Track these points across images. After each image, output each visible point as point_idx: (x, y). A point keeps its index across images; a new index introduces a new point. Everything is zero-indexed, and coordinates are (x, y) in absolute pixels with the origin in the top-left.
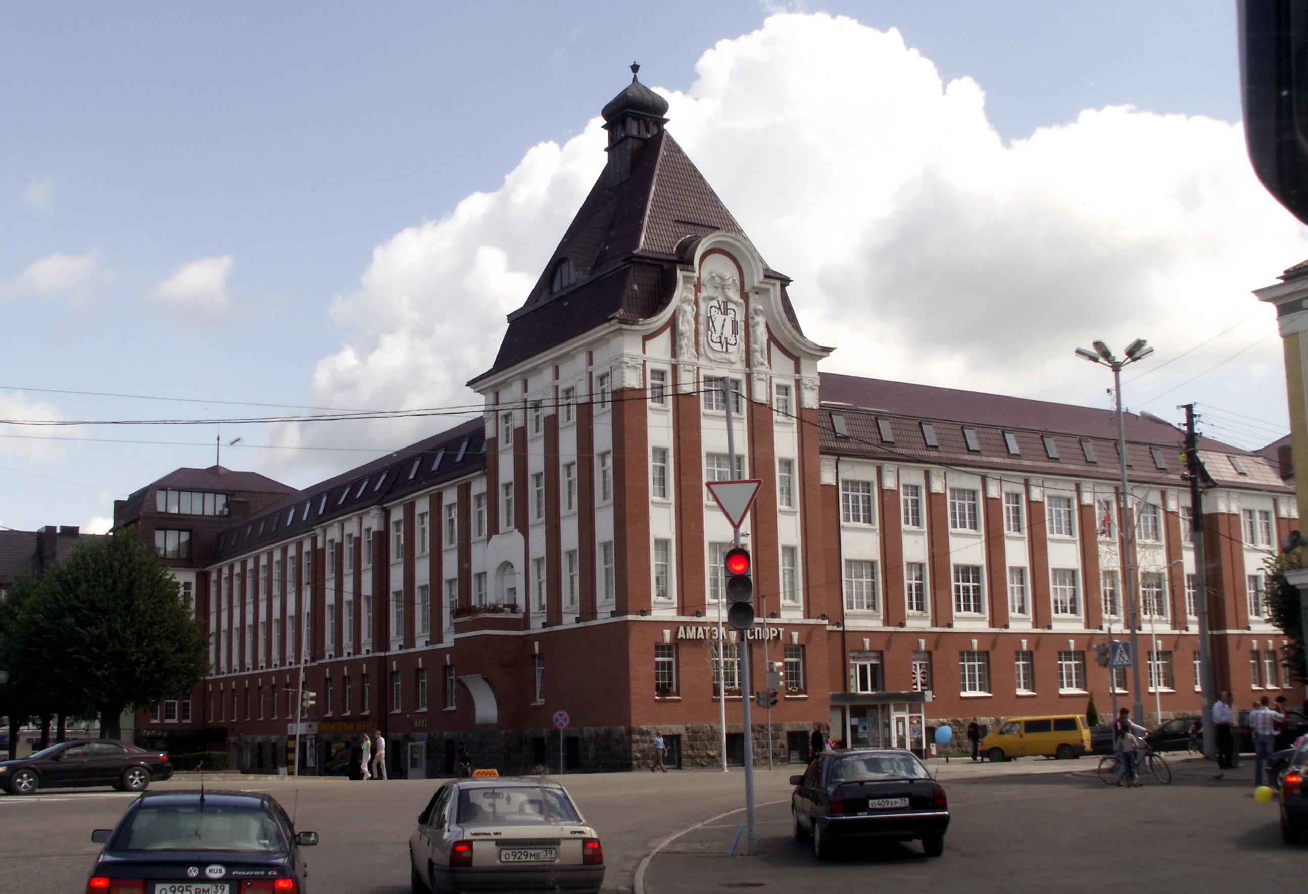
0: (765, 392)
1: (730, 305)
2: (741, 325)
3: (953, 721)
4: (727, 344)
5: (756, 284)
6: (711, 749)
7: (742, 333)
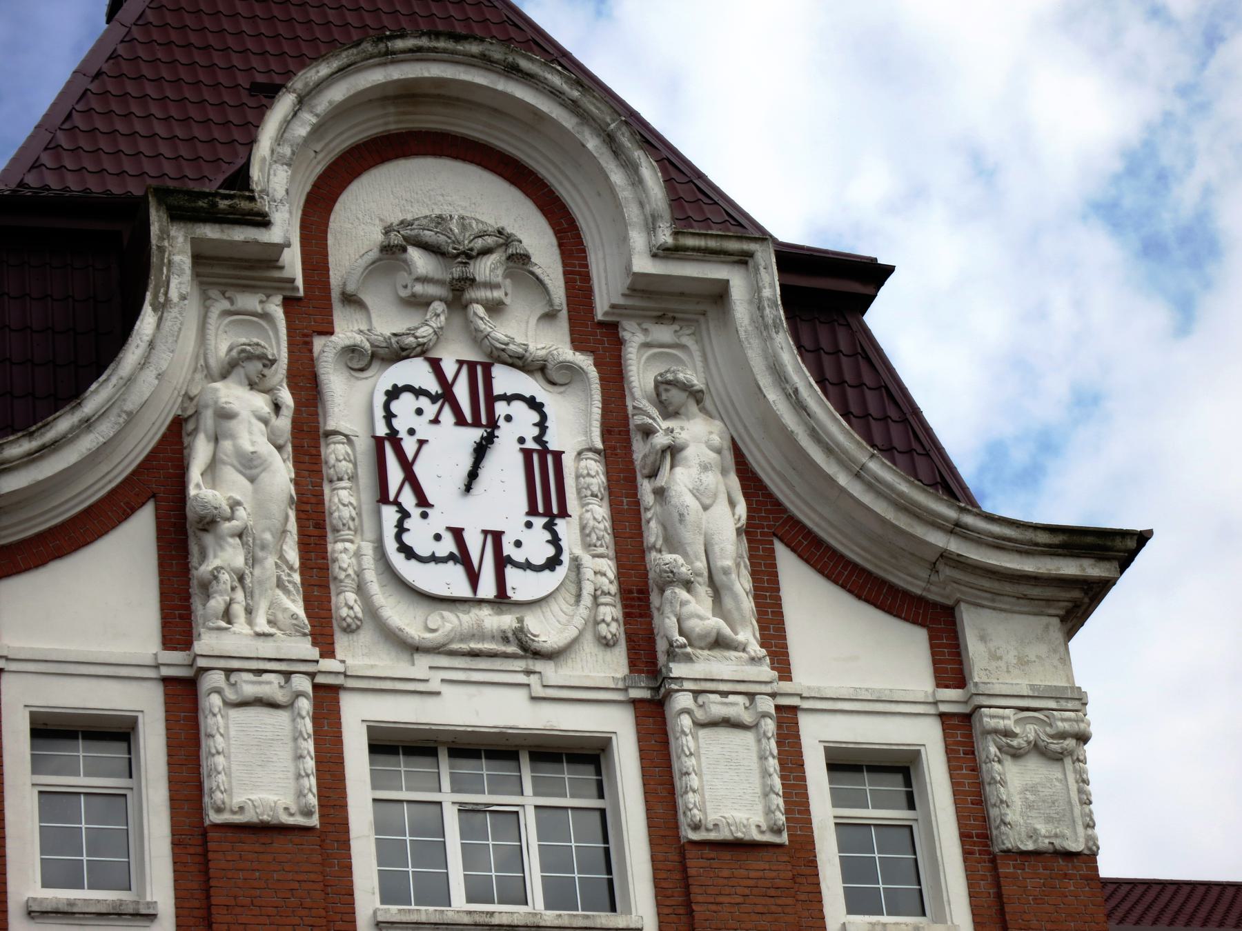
0: (754, 784)
1: (506, 380)
2: (585, 474)
4: (502, 562)
5: (643, 264)
7: (589, 513)
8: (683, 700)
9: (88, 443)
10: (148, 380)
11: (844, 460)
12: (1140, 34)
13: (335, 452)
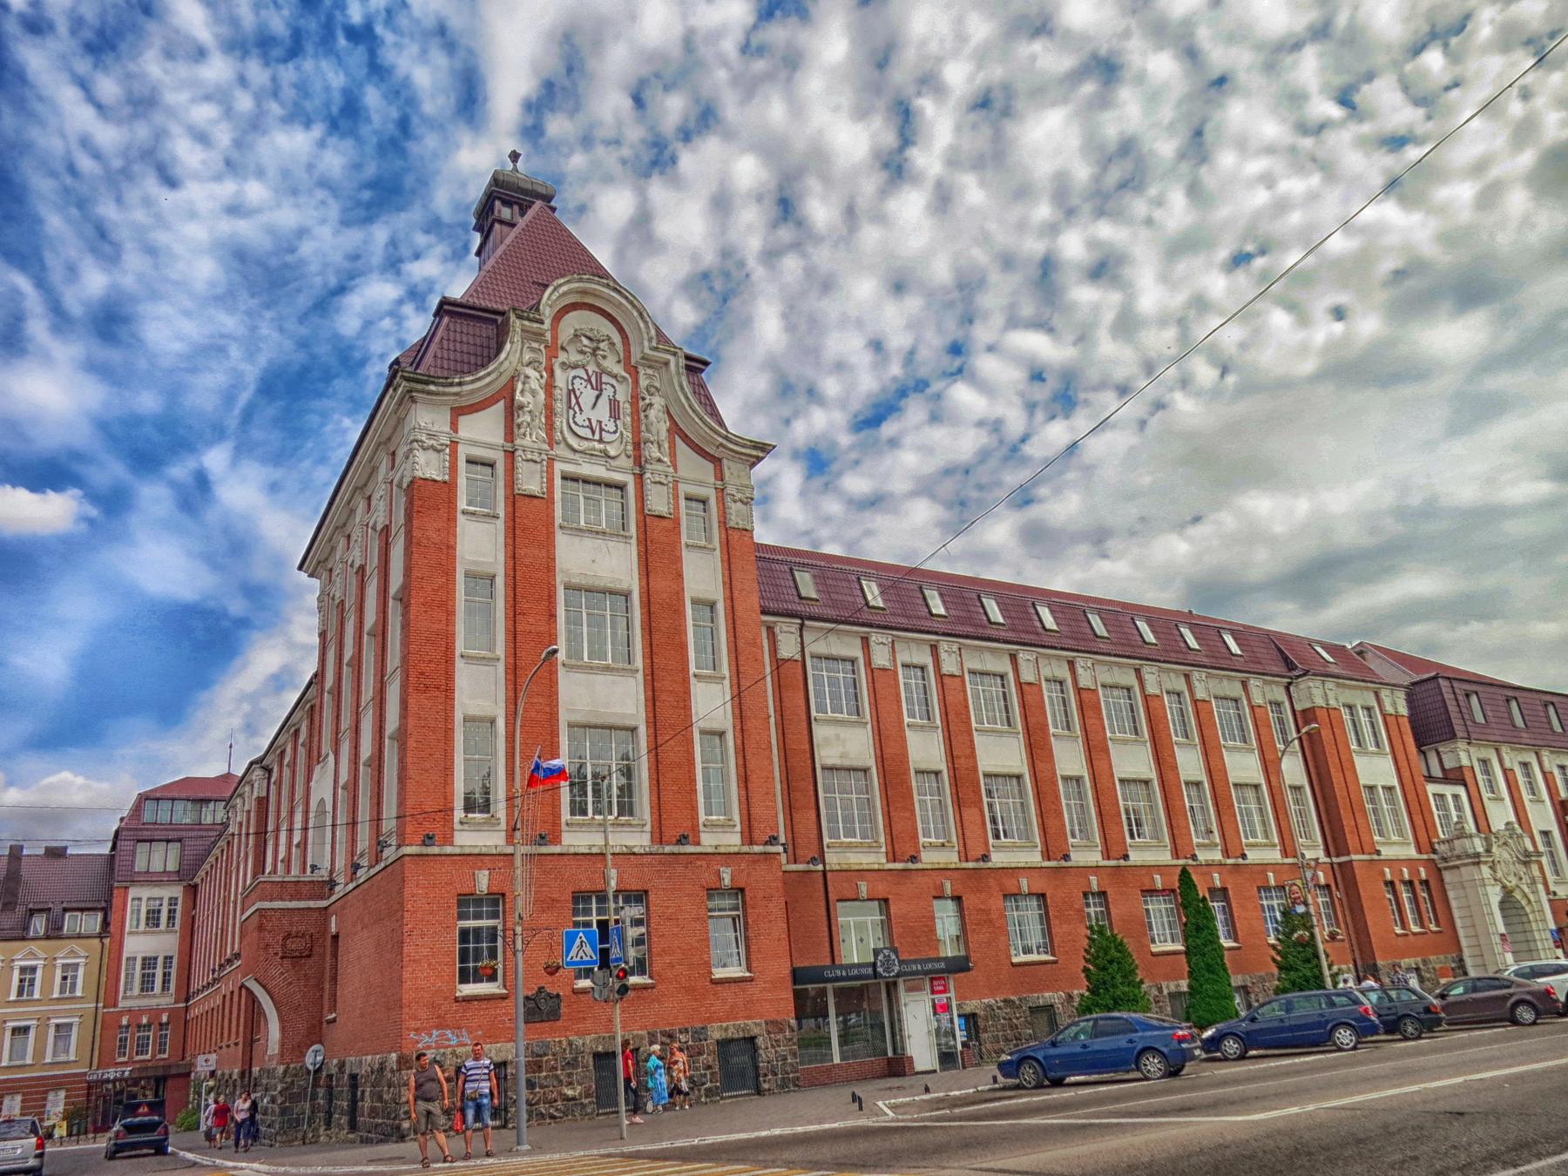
1: (605, 378)
2: (626, 408)
3: (1005, 1001)
4: (601, 430)
6: (570, 1084)
8: (648, 475)
9: (488, 380)
10: (506, 364)
11: (698, 415)
12: (705, 295)
13: (557, 392)
